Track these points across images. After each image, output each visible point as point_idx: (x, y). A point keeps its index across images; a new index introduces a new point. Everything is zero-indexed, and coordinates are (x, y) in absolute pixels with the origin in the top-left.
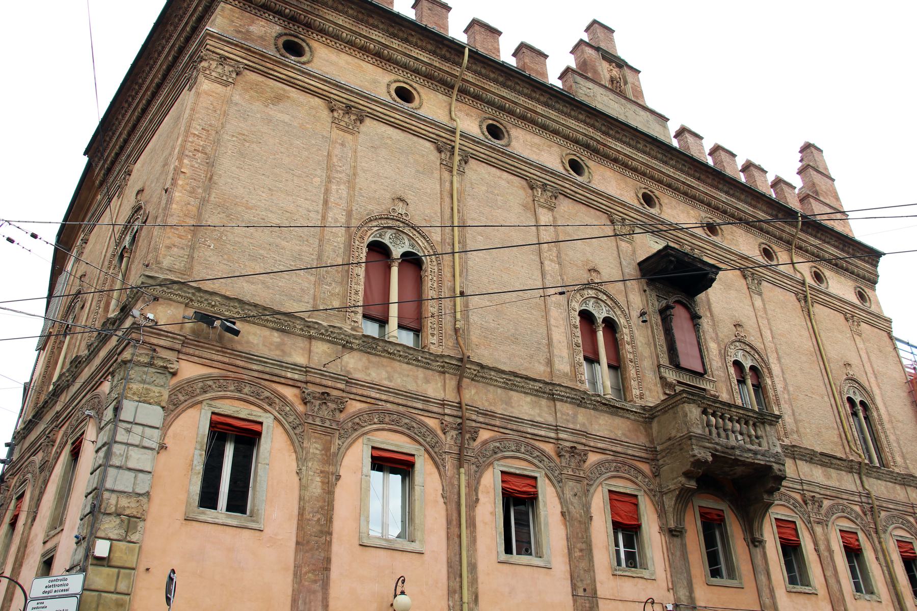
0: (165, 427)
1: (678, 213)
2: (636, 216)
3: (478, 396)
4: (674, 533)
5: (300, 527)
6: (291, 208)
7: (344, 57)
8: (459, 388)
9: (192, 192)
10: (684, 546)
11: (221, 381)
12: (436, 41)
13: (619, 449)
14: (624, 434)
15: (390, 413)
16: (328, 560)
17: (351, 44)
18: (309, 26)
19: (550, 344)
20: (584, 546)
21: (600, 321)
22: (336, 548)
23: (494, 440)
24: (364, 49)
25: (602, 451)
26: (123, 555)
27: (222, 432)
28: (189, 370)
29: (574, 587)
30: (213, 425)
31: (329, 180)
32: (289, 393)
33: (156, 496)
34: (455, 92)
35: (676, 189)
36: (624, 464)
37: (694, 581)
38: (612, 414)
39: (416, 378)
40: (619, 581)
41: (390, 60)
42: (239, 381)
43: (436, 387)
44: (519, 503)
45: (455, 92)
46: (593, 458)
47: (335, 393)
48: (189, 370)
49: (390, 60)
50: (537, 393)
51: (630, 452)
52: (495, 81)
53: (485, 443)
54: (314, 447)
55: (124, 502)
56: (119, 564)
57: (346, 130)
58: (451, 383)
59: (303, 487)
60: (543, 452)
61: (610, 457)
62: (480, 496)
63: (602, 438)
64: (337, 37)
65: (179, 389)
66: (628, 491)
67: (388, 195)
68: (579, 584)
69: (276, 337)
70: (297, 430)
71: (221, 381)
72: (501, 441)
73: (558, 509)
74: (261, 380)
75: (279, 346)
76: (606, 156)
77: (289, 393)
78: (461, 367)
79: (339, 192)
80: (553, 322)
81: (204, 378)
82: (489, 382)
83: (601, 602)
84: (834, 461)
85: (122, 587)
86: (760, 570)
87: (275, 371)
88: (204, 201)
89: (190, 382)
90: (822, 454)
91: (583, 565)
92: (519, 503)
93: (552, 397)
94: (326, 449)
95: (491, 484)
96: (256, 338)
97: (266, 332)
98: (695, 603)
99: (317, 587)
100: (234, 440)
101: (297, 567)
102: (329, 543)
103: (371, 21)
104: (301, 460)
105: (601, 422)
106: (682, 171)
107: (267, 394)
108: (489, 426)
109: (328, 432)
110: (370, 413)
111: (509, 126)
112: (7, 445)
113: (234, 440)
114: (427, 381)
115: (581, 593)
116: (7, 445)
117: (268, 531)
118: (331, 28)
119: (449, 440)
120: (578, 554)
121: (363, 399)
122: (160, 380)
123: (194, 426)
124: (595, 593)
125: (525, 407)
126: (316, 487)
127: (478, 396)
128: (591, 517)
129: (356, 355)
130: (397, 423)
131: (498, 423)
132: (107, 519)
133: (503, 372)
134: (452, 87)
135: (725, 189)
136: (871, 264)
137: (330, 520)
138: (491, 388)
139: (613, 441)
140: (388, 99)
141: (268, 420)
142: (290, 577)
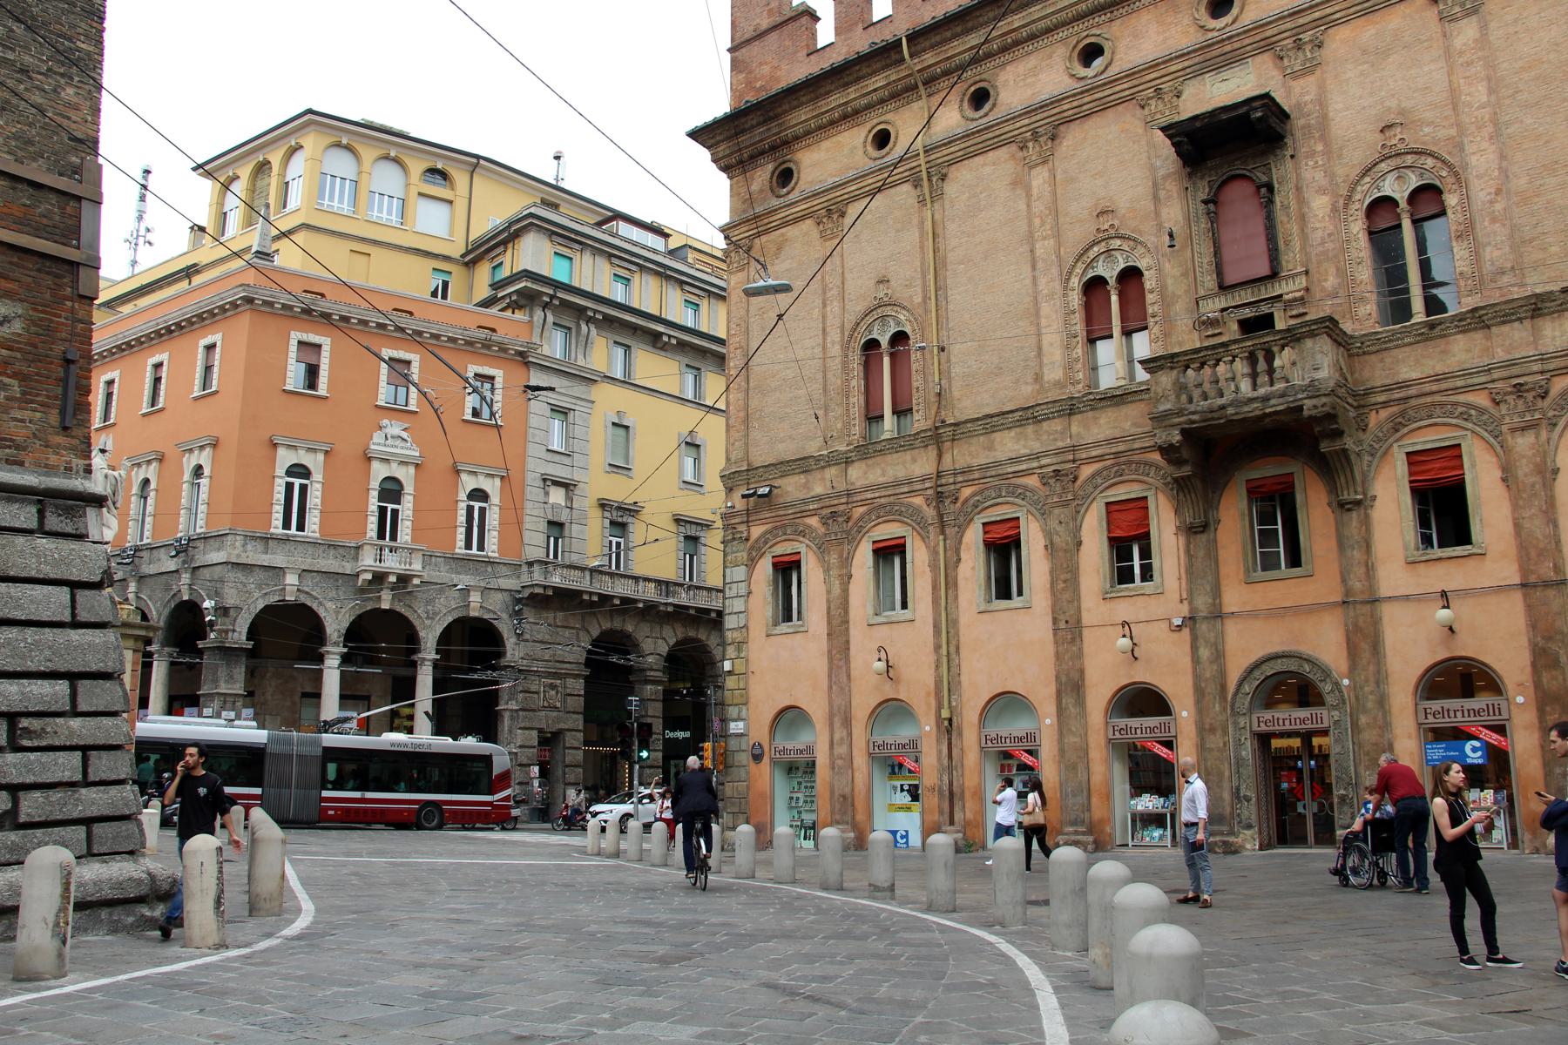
0: (750, 576)
2: (1180, 66)
3: (964, 455)
4: (1198, 528)
5: (829, 623)
7: (825, 144)
13: (1121, 447)
14: (1135, 425)
16: (848, 642)
17: (820, 128)
20: (1069, 576)
22: (853, 631)
24: (832, 123)
25: (1100, 458)
26: (740, 668)
28: (757, 531)
29: (1055, 621)
30: (775, 565)
32: (813, 521)
33: (751, 626)
34: (921, 87)
36: (1130, 463)
37: (1224, 582)
38: (1117, 405)
39: (904, 463)
41: (857, 112)
42: (784, 526)
44: (1003, 549)
45: (921, 87)
46: (1086, 471)
47: (842, 508)
49: (857, 112)
50: (1020, 423)
51: (1137, 446)
52: (955, 36)
54: (833, 558)
58: (932, 452)
59: (829, 592)
60: (1026, 488)
61: (1108, 463)
62: (963, 555)
64: (808, 133)
66: (1133, 496)
68: (1061, 617)
69: (802, 479)
73: (1042, 542)
74: (1000, 480)
81: (766, 532)
82: (971, 435)
83: (1086, 632)
92: (1003, 549)
95: (974, 537)
96: (792, 488)
97: (796, 478)
98: (1525, 596)
99: (842, 663)
101: (829, 652)
102: (847, 629)
103: (822, 91)
104: (827, 571)
105: (1102, 421)
107: (1461, 409)
110: (869, 513)
114: (914, 460)
115: (1062, 625)
118: (800, 130)
119: (930, 513)
120: (1061, 585)
121: (864, 503)
122: (742, 547)
124: (1079, 621)
126: (837, 590)
127: (964, 455)
128: (1079, 543)
129: (857, 464)
130: (890, 513)
131: (977, 475)
133: (978, 419)
134: (917, 87)
137: (846, 612)
138: (974, 440)
141: (803, 549)
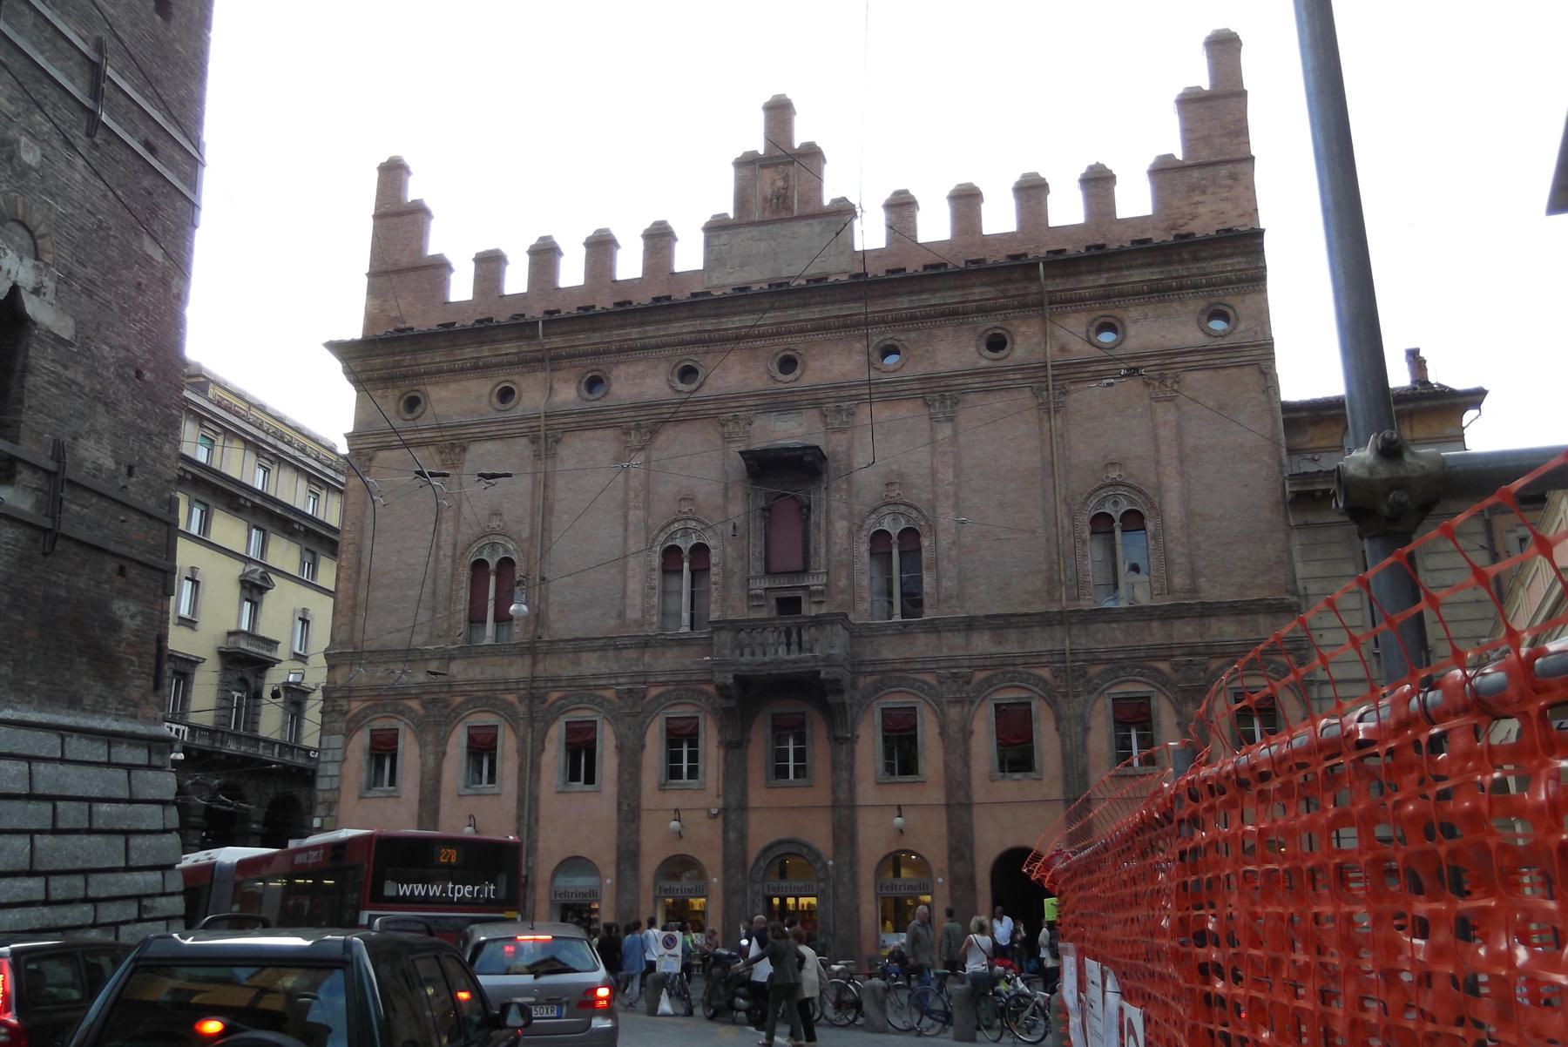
0: (346, 745)
1: (734, 374)
5: (422, 792)
7: (453, 386)
8: (534, 664)
18: (416, 375)
19: (624, 595)
21: (686, 552)
24: (463, 370)
29: (619, 804)
32: (414, 704)
35: (827, 329)
41: (487, 366)
43: (517, 670)
49: (487, 366)
56: (110, 772)
58: (528, 661)
63: (663, 673)
64: (439, 372)
65: (351, 720)
76: (1122, 295)
77: (414, 704)
80: (630, 573)
86: (844, 768)
90: (987, 617)
104: (422, 746)
106: (833, 302)
108: (554, 688)
119: (521, 709)
121: (462, 693)
125: (592, 664)
126: (431, 761)
127: (550, 666)
129: (459, 662)
132: (58, 741)
139: (673, 672)
141: (401, 727)
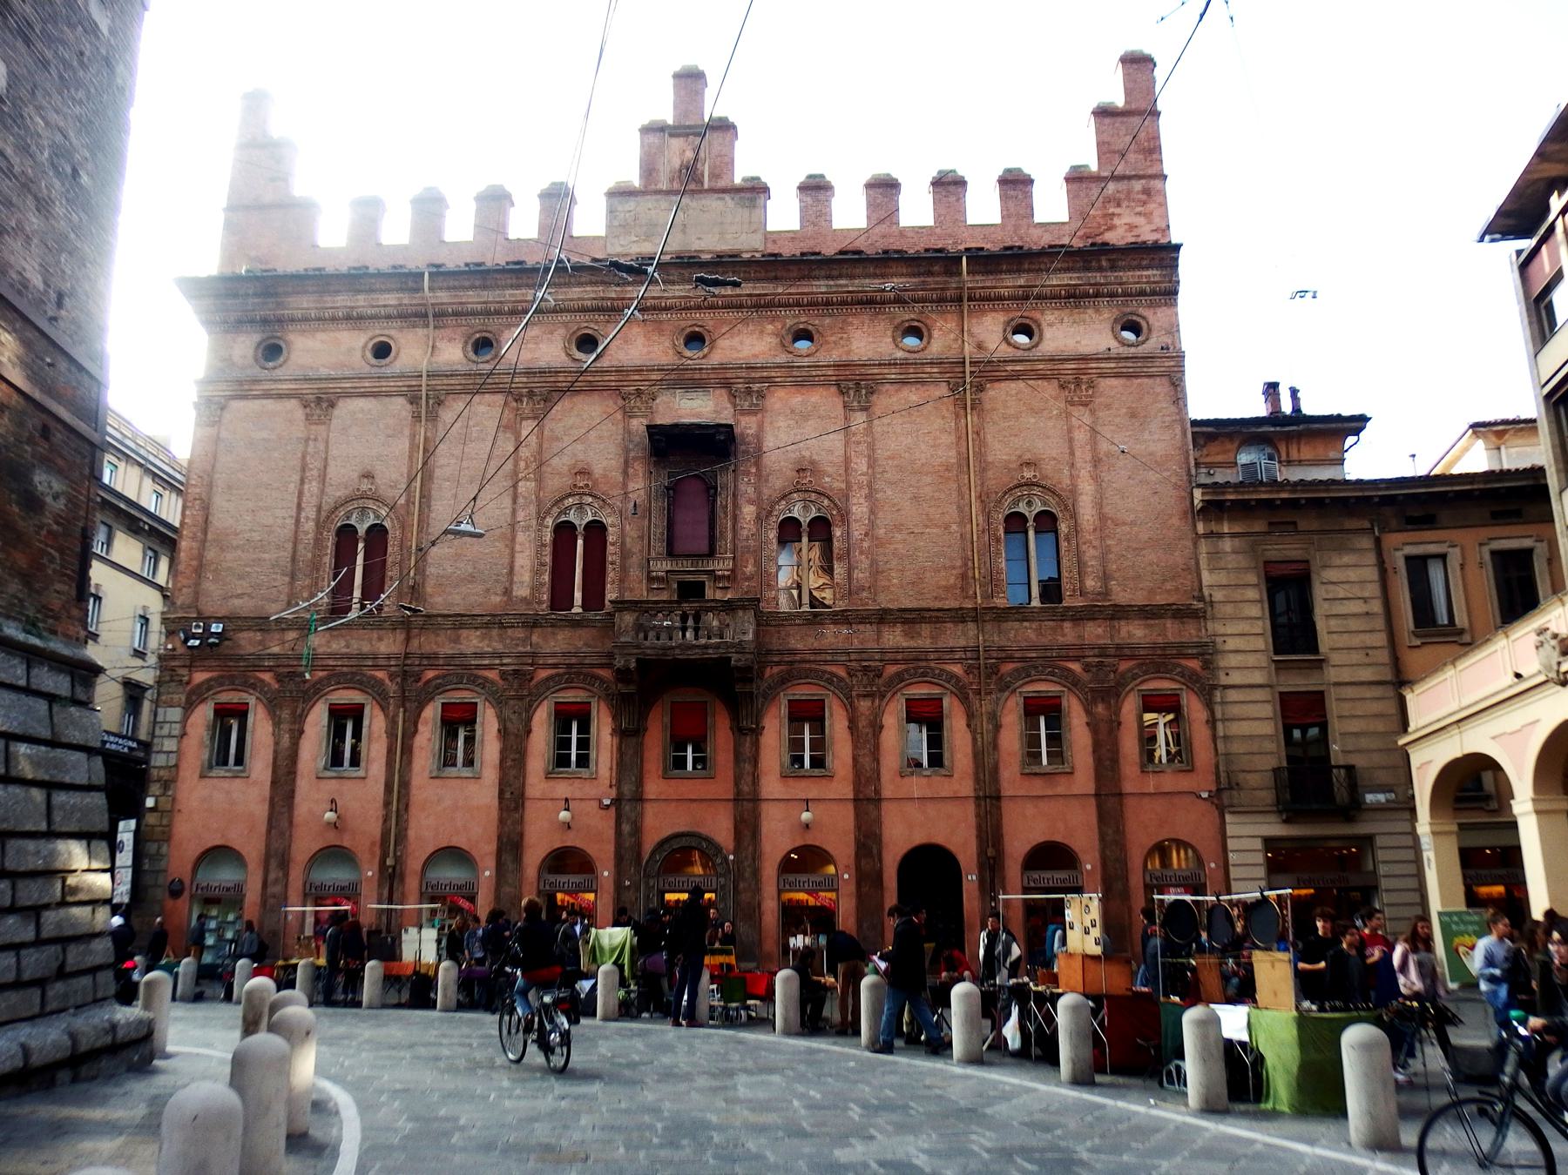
5: (274, 772)
6: (270, 521)
9: (194, 538)
10: (639, 753)
11: (219, 681)
12: (905, 622)
14: (586, 645)
15: (345, 674)
16: (293, 791)
23: (437, 677)
27: (223, 713)
28: (200, 677)
29: (501, 793)
31: (302, 481)
32: (267, 677)
39: (370, 640)
40: (552, 783)
43: (388, 645)
48: (200, 677)
53: (429, 681)
54: (285, 714)
55: (162, 773)
57: (319, 422)
59: (277, 743)
64: (306, 319)
67: (356, 475)
70: (273, 705)
71: (219, 681)
72: (444, 676)
75: (260, 642)
77: (267, 677)
78: (413, 621)
79: (312, 488)
80: (518, 548)
84: (927, 615)
85: (165, 822)
87: (256, 663)
88: (204, 541)
89: (200, 685)
91: (513, 772)
93: (502, 626)
94: (293, 713)
100: (230, 716)
102: (294, 780)
109: (294, 700)
110: (328, 678)
111: (1037, 315)
112: (692, 151)
113: (230, 716)
114: (380, 639)
116: (692, 151)
117: (253, 776)
119: (392, 687)
123: (204, 714)
126: (286, 740)
127: (426, 643)
130: (351, 681)
135: (823, 273)
136: (1161, 267)
140: (367, 369)
142: (266, 807)
